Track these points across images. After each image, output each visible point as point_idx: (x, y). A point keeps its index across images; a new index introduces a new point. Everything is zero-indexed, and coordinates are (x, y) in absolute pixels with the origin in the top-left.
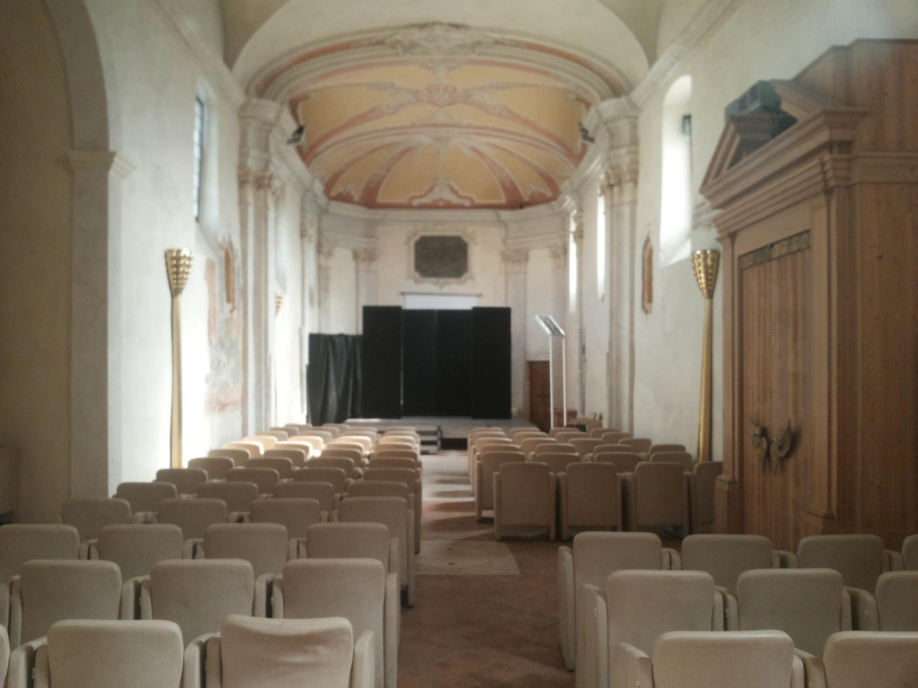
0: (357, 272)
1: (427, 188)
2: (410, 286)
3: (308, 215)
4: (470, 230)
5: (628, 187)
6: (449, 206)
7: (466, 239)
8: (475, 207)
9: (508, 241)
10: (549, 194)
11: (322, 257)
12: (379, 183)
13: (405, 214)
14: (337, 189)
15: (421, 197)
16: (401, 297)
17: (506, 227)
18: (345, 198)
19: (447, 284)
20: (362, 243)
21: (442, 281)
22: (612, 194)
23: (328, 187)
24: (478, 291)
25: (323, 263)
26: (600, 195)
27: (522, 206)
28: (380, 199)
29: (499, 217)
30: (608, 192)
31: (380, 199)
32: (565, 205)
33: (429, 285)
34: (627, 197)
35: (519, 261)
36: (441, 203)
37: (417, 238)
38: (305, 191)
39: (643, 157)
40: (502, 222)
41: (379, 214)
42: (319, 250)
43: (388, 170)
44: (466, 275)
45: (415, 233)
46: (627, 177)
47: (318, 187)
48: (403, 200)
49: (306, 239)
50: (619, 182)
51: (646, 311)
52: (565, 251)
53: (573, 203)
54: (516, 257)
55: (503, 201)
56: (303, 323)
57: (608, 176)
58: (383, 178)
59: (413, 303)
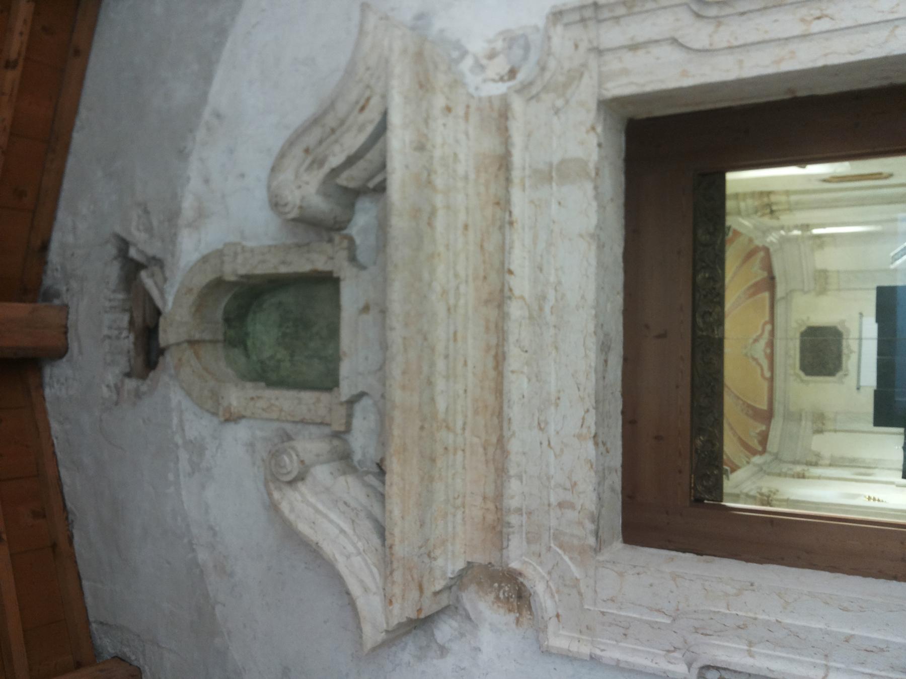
0: (835, 431)
1: (754, 363)
2: (851, 381)
3: (784, 470)
4: (794, 325)
5: (773, 198)
6: (771, 344)
7: (803, 329)
8: (772, 320)
9: (806, 289)
10: (762, 254)
11: (821, 462)
12: (749, 406)
13: (779, 383)
14: (755, 444)
15: (762, 370)
16: (862, 390)
17: (792, 291)
18: (764, 439)
19: (848, 346)
20: (807, 425)
21: (845, 351)
22: (779, 210)
23: (754, 453)
24: (857, 316)
25: (828, 462)
26: (778, 219)
27: (772, 278)
28: (764, 406)
29: (783, 298)
30: (777, 214)
31: (764, 406)
32: (774, 240)
33: (850, 363)
34: (783, 198)
35: (826, 278)
36: (768, 351)
37: (802, 374)
38: (762, 470)
39: (748, 189)
40: (787, 294)
41: (778, 408)
42: (816, 465)
43: (738, 398)
44: (840, 328)
45: (798, 376)
46: (766, 200)
47: (757, 459)
48: (765, 385)
49: (807, 474)
50: (769, 205)
51: (890, 175)
52: (819, 236)
53: (774, 234)
54: (822, 281)
55: (766, 295)
56: (892, 483)
57: (763, 215)
58: (744, 403)
59: (870, 378)
